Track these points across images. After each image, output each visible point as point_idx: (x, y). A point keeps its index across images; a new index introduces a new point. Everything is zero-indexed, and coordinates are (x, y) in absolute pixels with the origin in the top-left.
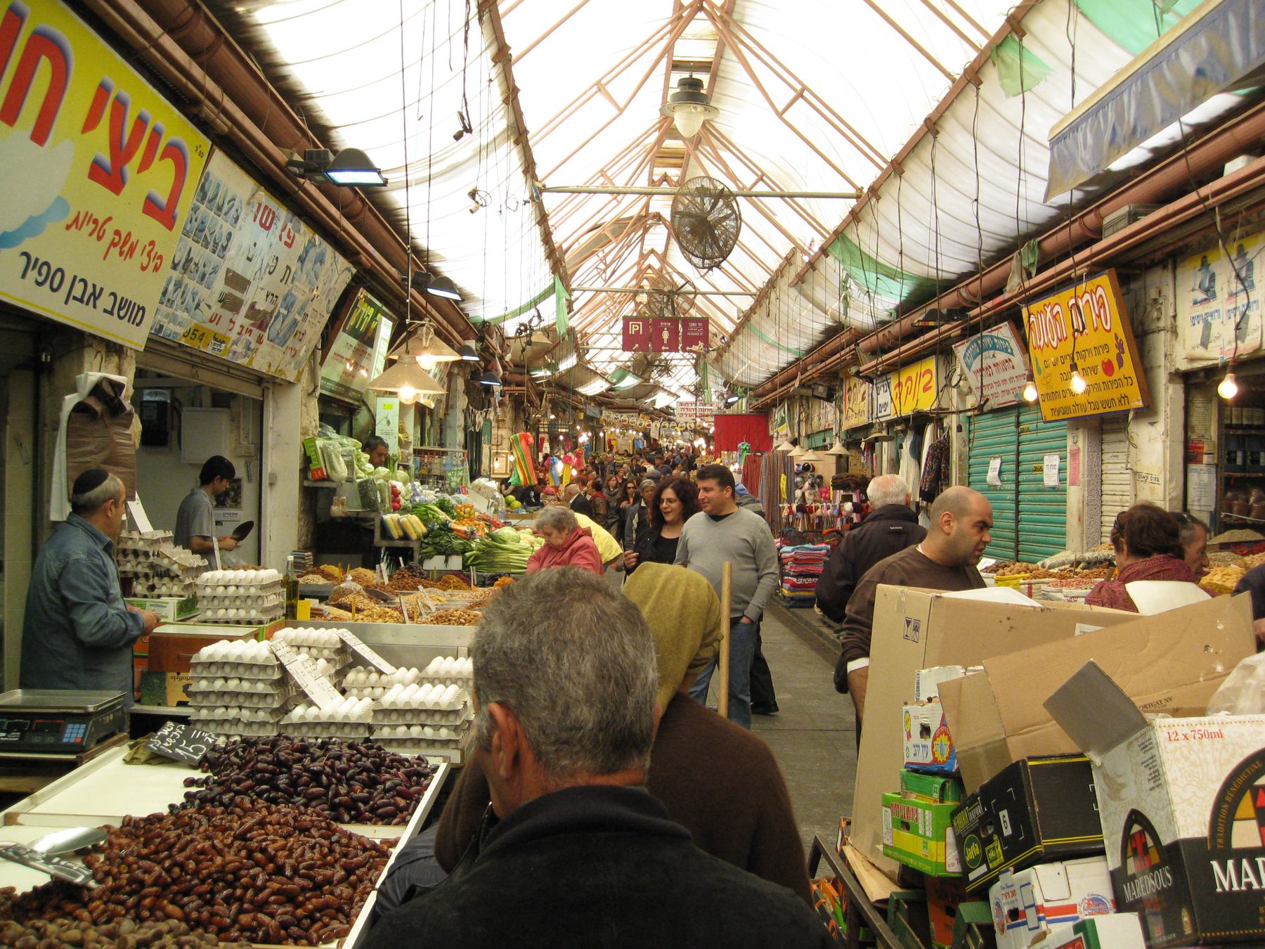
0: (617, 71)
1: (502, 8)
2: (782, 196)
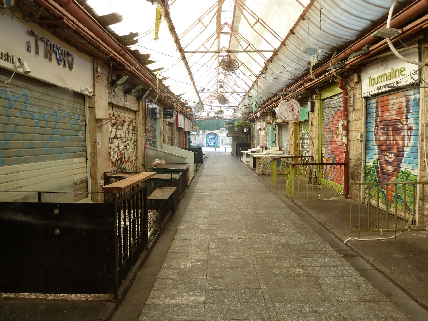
1: (169, 2)
2: (257, 52)
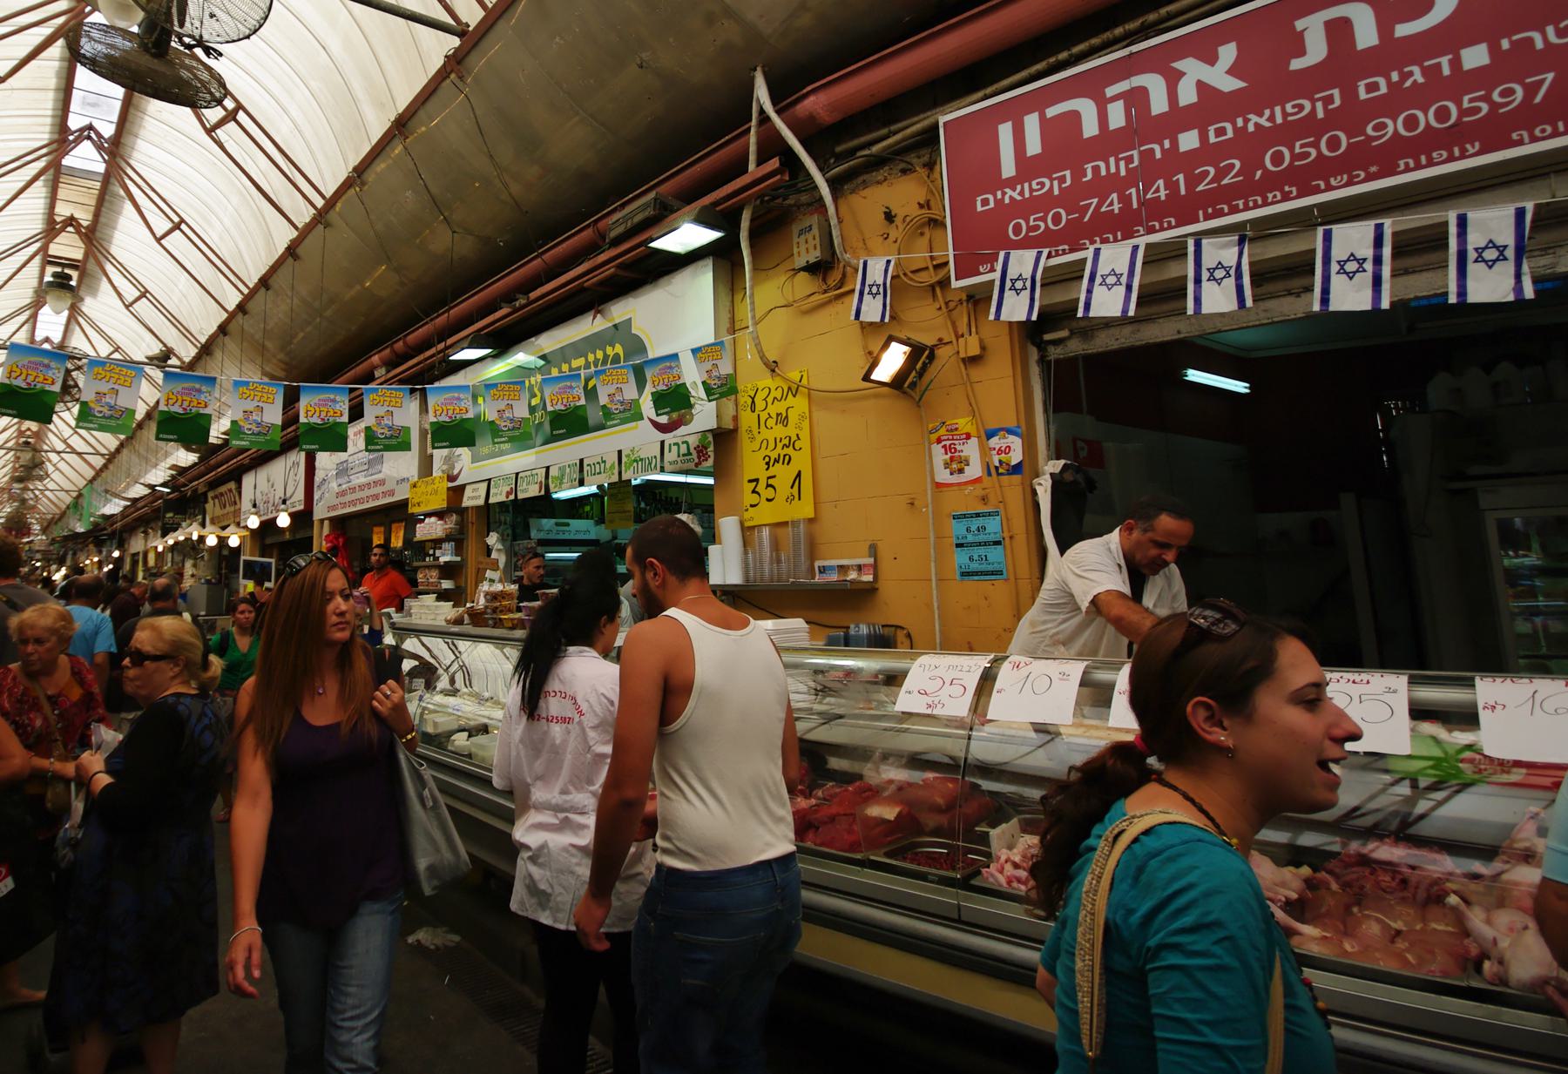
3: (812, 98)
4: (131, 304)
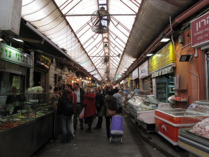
0: (99, 52)
3: (176, 20)
4: (116, 26)
